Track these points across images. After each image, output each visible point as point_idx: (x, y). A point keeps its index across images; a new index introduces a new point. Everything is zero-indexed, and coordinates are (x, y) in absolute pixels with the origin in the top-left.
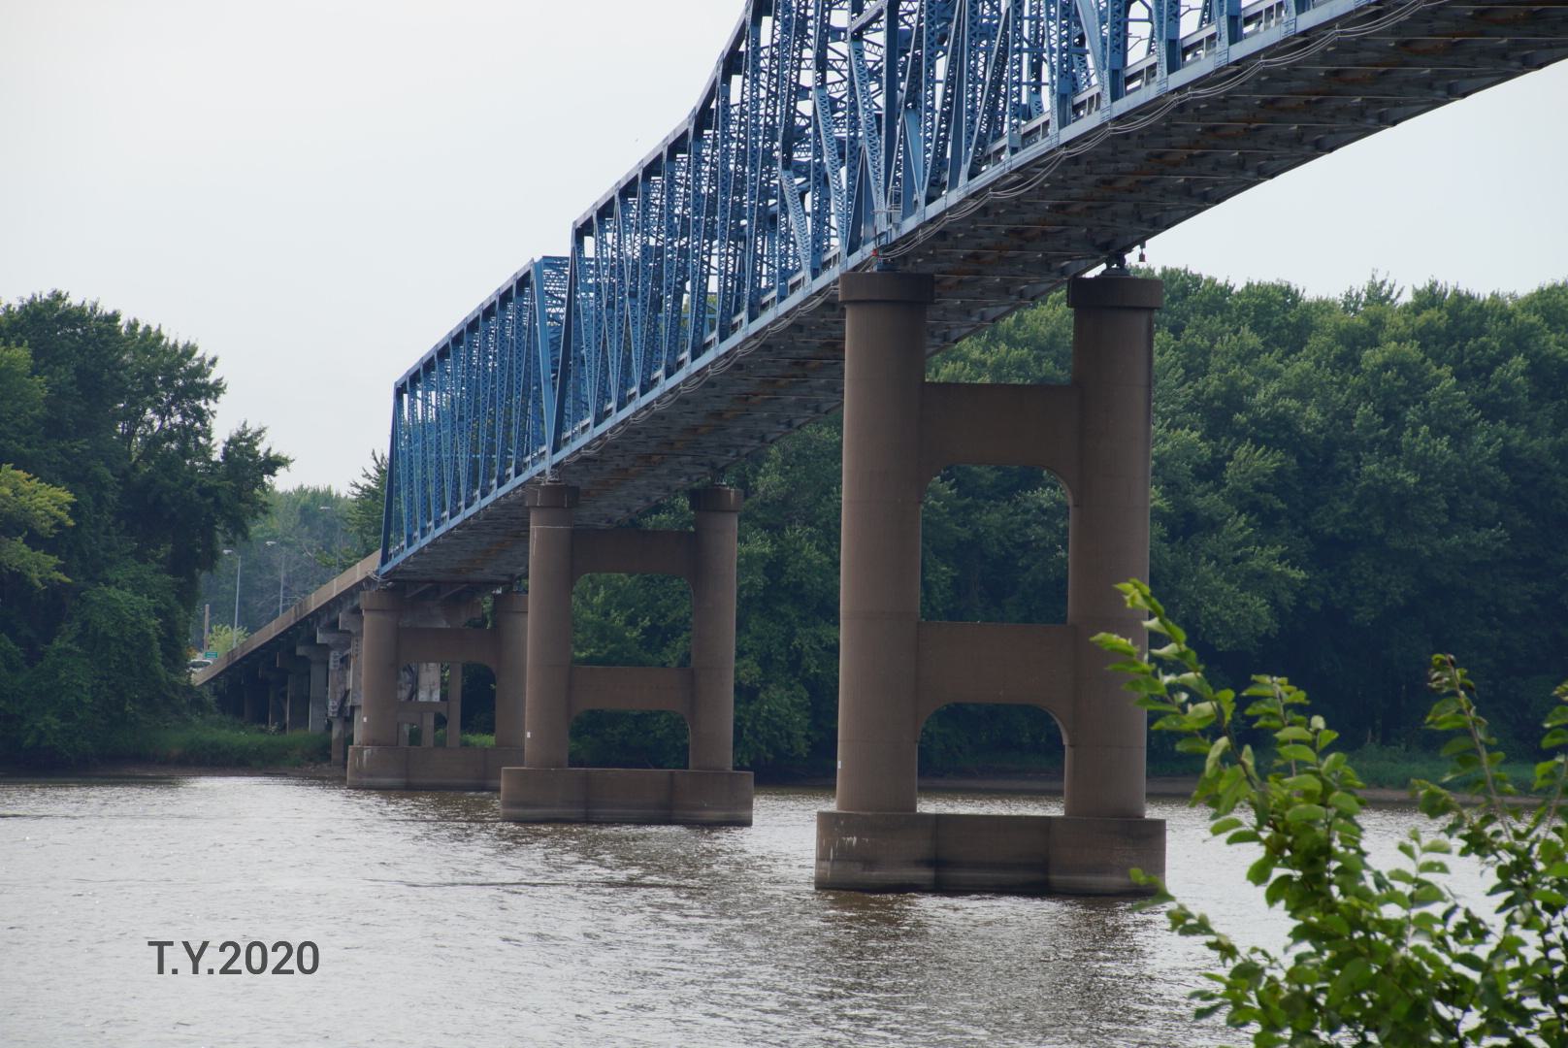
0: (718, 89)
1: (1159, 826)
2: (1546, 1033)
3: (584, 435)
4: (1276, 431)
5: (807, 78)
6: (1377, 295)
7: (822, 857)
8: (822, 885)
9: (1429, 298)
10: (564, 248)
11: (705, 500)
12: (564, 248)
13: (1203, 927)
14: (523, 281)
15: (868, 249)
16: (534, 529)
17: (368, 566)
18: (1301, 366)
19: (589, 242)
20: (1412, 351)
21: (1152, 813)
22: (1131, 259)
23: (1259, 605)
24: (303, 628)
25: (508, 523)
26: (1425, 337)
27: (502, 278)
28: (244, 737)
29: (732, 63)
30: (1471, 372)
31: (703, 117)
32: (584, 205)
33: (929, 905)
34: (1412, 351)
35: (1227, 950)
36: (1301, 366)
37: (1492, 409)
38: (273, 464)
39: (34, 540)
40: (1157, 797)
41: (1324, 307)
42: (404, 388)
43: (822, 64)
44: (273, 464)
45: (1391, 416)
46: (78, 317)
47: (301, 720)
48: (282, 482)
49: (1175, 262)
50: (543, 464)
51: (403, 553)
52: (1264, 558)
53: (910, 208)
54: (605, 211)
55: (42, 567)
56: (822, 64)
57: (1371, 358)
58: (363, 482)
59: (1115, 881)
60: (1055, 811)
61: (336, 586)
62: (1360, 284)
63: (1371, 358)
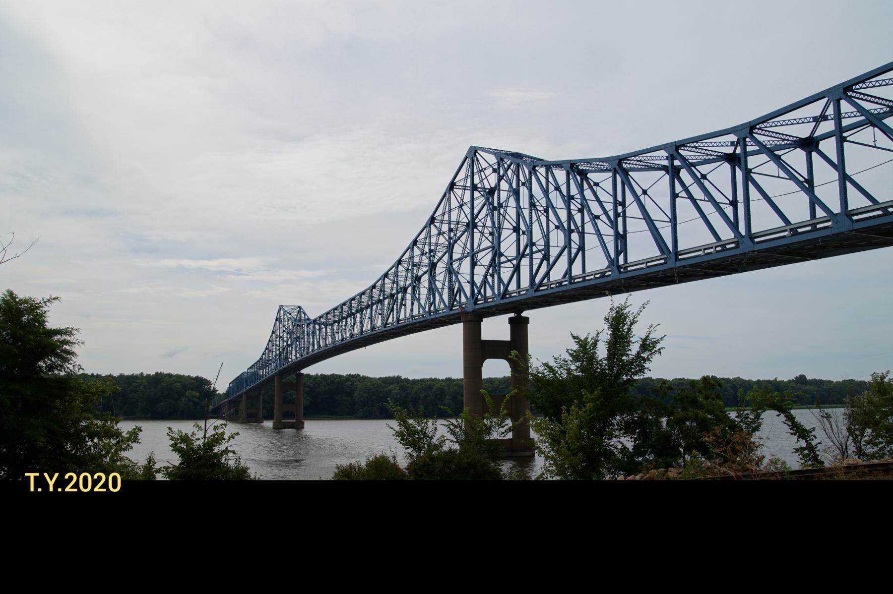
0: (262, 356)
1: (304, 422)
2: (888, 443)
3: (248, 387)
4: (309, 386)
5: (271, 355)
6: (317, 375)
7: (273, 425)
8: (273, 428)
9: (322, 375)
10: (246, 371)
11: (259, 394)
12: (246, 371)
13: (392, 428)
14: (242, 374)
15: (277, 371)
16: (243, 396)
17: (227, 400)
18: (311, 381)
19: (249, 370)
20: (320, 379)
21: (303, 421)
22: (301, 372)
23: (308, 402)
24: (220, 406)
25: (241, 396)
26: (321, 378)
27: (240, 373)
28: (214, 416)
29: (263, 354)
30: (325, 381)
31: (260, 359)
32: (249, 367)
33: (284, 430)
34: (320, 379)
35: (394, 430)
36: (311, 381)
37: (328, 384)
38: (217, 391)
39: (196, 398)
40: (304, 419)
41: (312, 376)
42: (230, 383)
43: (272, 354)
44: (217, 391)
45: (319, 385)
46: (200, 378)
47: (219, 414)
48: (218, 392)
49: (307, 373)
50: (244, 390)
51: (230, 398)
52: (308, 398)
53: (281, 367)
54: (251, 367)
55: (197, 400)
56: (272, 354)
57: (317, 380)
58: (607, 346)
59: (300, 427)
60: (295, 421)
61: (223, 402)
62: (316, 374)
63: (317, 380)
